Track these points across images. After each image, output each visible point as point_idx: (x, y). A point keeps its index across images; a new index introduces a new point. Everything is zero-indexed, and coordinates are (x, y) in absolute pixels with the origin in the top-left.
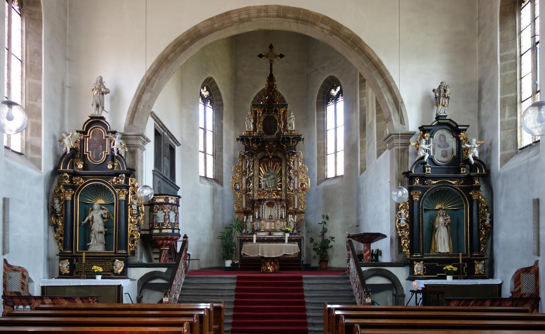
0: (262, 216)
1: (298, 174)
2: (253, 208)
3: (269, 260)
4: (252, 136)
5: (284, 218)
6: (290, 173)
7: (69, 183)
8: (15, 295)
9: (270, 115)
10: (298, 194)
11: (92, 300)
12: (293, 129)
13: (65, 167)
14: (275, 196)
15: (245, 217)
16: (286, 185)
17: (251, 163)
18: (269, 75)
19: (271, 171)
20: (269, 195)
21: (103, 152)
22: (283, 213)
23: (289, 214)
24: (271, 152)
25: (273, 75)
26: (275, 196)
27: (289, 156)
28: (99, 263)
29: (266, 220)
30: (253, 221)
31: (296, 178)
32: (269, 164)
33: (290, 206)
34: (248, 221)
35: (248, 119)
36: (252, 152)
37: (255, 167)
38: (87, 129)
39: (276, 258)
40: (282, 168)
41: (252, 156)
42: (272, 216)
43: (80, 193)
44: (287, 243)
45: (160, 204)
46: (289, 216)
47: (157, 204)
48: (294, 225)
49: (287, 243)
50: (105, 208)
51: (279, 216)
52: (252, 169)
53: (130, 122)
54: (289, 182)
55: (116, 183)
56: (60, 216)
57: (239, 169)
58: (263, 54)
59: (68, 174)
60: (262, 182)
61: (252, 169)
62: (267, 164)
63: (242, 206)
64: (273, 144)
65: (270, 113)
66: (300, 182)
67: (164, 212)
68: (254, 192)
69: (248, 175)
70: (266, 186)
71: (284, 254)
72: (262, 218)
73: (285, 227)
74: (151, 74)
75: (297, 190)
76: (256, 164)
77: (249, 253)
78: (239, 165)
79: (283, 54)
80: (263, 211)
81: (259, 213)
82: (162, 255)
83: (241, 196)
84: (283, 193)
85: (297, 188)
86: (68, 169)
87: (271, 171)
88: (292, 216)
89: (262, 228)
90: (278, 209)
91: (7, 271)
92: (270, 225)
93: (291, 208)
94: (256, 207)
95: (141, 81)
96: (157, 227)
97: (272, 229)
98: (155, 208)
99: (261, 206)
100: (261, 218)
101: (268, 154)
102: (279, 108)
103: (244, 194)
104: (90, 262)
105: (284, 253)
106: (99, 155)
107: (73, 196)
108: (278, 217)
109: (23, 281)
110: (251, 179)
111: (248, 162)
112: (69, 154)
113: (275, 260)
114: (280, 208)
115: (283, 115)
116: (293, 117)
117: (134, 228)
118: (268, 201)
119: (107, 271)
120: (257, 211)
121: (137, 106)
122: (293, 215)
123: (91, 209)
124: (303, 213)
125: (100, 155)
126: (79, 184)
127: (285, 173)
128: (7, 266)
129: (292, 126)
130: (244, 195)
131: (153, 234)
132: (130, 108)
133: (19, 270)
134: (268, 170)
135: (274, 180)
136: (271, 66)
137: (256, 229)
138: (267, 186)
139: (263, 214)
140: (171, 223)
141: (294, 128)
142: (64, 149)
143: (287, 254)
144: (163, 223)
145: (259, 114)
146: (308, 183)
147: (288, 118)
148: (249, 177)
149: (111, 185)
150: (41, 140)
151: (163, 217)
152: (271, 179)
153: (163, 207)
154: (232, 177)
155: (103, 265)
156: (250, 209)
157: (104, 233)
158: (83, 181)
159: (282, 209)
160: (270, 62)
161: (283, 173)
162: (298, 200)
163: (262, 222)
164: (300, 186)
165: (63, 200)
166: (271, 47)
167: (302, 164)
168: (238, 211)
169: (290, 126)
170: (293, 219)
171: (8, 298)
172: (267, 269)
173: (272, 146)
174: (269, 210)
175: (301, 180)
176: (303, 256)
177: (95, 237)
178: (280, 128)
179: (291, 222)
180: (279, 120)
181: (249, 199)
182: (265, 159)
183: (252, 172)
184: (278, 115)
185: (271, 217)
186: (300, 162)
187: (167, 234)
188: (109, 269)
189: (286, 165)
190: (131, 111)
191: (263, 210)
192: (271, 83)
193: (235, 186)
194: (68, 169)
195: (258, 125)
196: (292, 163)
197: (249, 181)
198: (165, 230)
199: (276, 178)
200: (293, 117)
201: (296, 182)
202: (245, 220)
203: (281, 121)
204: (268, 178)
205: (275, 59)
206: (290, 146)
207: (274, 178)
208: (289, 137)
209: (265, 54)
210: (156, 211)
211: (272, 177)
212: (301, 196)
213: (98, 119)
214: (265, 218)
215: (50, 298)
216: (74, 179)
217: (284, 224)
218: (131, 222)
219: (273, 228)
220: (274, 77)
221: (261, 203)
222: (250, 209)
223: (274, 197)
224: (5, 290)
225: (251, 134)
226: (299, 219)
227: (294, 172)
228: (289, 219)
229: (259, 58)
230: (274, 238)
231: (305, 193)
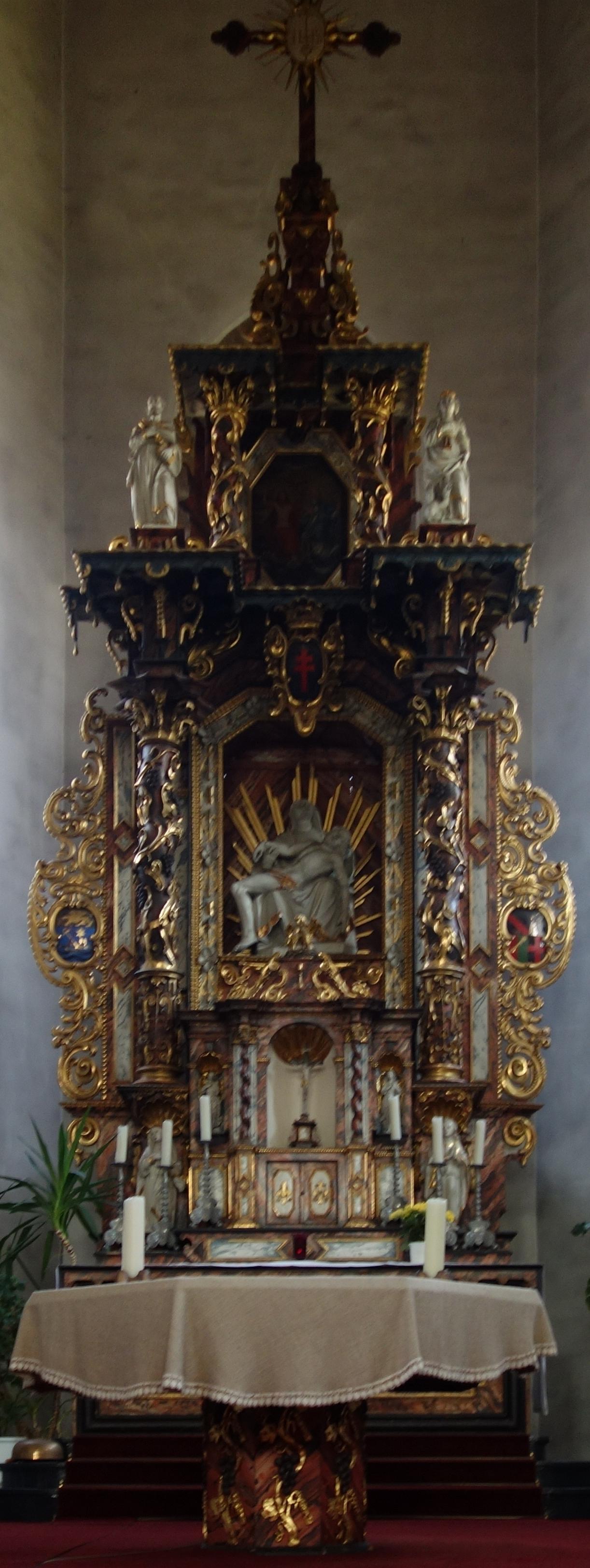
0: (246, 1123)
1: (493, 845)
2: (180, 1073)
3: (267, 1433)
4: (169, 556)
5: (397, 1135)
6: (436, 829)
9: (300, 449)
10: (493, 983)
12: (458, 516)
14: (333, 985)
15: (123, 1133)
16: (412, 913)
17: (165, 755)
18: (296, 170)
19: (306, 826)
20: (294, 979)
22: (394, 1102)
23: (430, 1114)
24: (304, 696)
25: (318, 169)
26: (333, 985)
27: (434, 704)
29: (277, 1151)
30: (185, 1160)
31: (480, 876)
32: (296, 784)
33: (440, 1060)
34: (145, 1159)
35: (142, 449)
37: (198, 798)
39: (335, 1412)
40: (381, 810)
41: (172, 709)
42: (312, 1126)
44: (439, 1275)
46: (437, 1122)
48: (471, 1192)
49: (439, 1275)
51: (365, 1126)
52: (172, 800)
54: (432, 889)
57: (85, 812)
58: (252, 24)
60: (247, 903)
61: (172, 800)
62: (282, 788)
63: (110, 1064)
64: (322, 632)
65: (297, 436)
66: (505, 899)
68: (194, 969)
69: (142, 839)
70: (276, 930)
71: (419, 1382)
72: (244, 1138)
73: (404, 1202)
75: (488, 957)
76: (205, 774)
77: (81, 1373)
78: (91, 782)
79: (392, 26)
80: (252, 1091)
81: (222, 1110)
83: (101, 1000)
84: (389, 979)
85: (484, 946)
87: (306, 826)
88: (451, 1125)
89: (244, 1208)
90: (357, 1075)
92: (303, 1189)
93: (446, 1073)
94: (206, 1061)
97: (313, 1217)
99: (237, 1057)
100: (236, 1137)
101: (287, 709)
102: (364, 384)
103: (123, 983)
105: (419, 1366)
108: (357, 1133)
110: (166, 872)
111: (146, 752)
113: (331, 1434)
114: (372, 1070)
115: (387, 440)
116: (459, 438)
118: (288, 1020)
120: (213, 1088)
122: (458, 1119)
124: (528, 1111)
127: (407, 838)
129: (456, 499)
130: (122, 989)
134: (287, 824)
135: (326, 888)
136: (307, 106)
137: (197, 1215)
138: (279, 924)
139: (252, 1114)
141: (465, 510)
143: (446, 1374)
145: (225, 425)
146: (558, 905)
147: (428, 441)
148: (156, 855)
152: (311, 881)
154: (43, 866)
156: (161, 1077)
159: (384, 1078)
160: (302, 80)
161: (390, 836)
162: (493, 1027)
163: (245, 1164)
164: (503, 930)
167: (517, 779)
168: (79, 1099)
169: (439, 497)
170: (459, 1150)
172: (255, 1516)
173: (315, 645)
174: (296, 1083)
175: (511, 889)
176: (538, 1409)
179: (451, 1168)
180: (365, 465)
181: (152, 1009)
182: (268, 757)
183: (171, 817)
184: (350, 444)
185: (304, 1134)
186: (510, 766)
189: (415, 773)
191: (253, 1077)
193: (59, 927)
195: (217, 505)
196: (451, 758)
197: (150, 881)
199: (341, 875)
200: (459, 438)
201: (479, 901)
202: (121, 1156)
203: (379, 474)
204: (284, 871)
206: (441, 639)
207: (327, 875)
208: (434, 565)
211: (314, 863)
212: (514, 999)
214: (262, 1136)
217: (401, 1182)
219: (321, 1207)
220: (328, 181)
221: (237, 1035)
222: (161, 1077)
223: (327, 994)
226: (501, 1152)
227: (468, 831)
228: (431, 1146)
229: (220, 52)
231: (540, 978)
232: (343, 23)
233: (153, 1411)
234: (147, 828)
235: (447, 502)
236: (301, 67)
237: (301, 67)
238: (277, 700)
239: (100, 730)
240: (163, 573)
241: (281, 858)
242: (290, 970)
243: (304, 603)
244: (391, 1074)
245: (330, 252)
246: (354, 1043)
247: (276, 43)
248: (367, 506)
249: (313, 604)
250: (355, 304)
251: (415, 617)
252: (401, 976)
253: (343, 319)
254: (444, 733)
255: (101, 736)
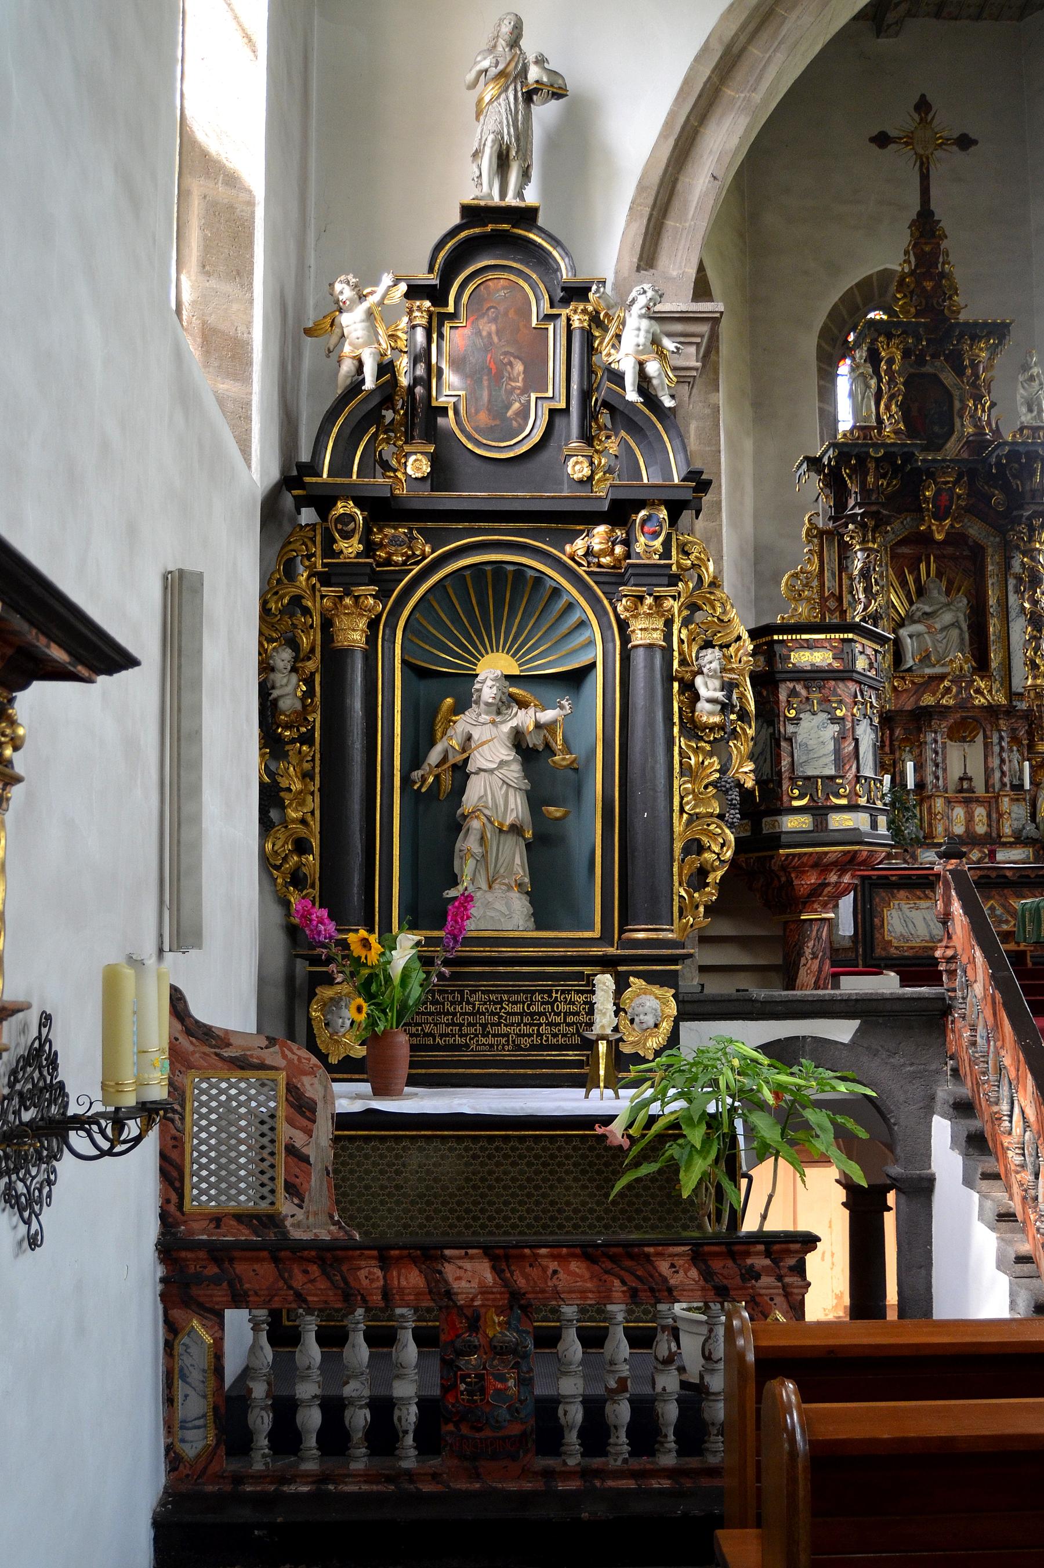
7: (359, 555)
8: (245, 1235)
9: (924, 370)
11: (767, 1262)
13: (341, 467)
18: (919, 214)
20: (959, 692)
21: (533, 396)
25: (932, 214)
28: (514, 998)
32: (923, 567)
36: (878, 512)
38: (448, 274)
42: (970, 779)
43: (406, 613)
45: (814, 677)
47: (798, 680)
50: (856, 638)
53: (640, 259)
55: (605, 560)
56: (293, 741)
58: (893, 133)
59: (359, 502)
64: (956, 483)
67: (835, 720)
74: (743, 27)
78: (809, 568)
79: (972, 136)
82: (808, 951)
86: (354, 477)
90: (1002, 749)
91: (190, 1067)
92: (970, 819)
95: (698, 59)
96: (801, 797)
98: (783, 696)
104: (461, 993)
106: (510, 413)
107: (373, 624)
109: (299, 1139)
112: (372, 392)
117: (699, 801)
119: (561, 1040)
121: (674, 182)
123: (449, 701)
125: (517, 414)
126: (404, 563)
128: (189, 1032)
131: (784, 839)
132: (641, 188)
133: (268, 1062)
140: (808, 778)
142: (347, 366)
144: (832, 778)
145: (890, 362)
149: (580, 570)
150: (251, 301)
151: (831, 746)
153: (826, 691)
155: (534, 1008)
157: (529, 835)
158: (428, 549)
160: (922, 164)
165: (312, 650)
166: (923, 106)
169: (1030, 410)
171: (202, 1254)
173: (951, 490)
177: (484, 856)
178: (980, 419)
187: (853, 837)
188: (572, 1030)
190: (650, 201)
192: (926, 244)
194: (354, 477)
198: (846, 816)
205: (939, 153)
209: (902, 134)
210: (792, 713)
211: (947, 618)
213: (506, 227)
215: (489, 1252)
216: (378, 538)
218: (686, 770)
223: (979, 701)
224: (174, 1198)
225: (871, 439)
230: (1009, 874)
232: (945, 134)
233: (906, 954)
234: (863, 600)
235: (1035, 413)
236: (921, 157)
237: (921, 157)
238: (924, 520)
239: (815, 537)
240: (880, 455)
241: (925, 613)
242: (957, 686)
243: (948, 467)
244: (1015, 748)
245: (941, 260)
246: (999, 731)
247: (907, 144)
248: (976, 409)
249: (953, 468)
250: (957, 289)
251: (1015, 477)
252: (1001, 685)
253: (950, 298)
254: (1038, 546)
255: (816, 540)
